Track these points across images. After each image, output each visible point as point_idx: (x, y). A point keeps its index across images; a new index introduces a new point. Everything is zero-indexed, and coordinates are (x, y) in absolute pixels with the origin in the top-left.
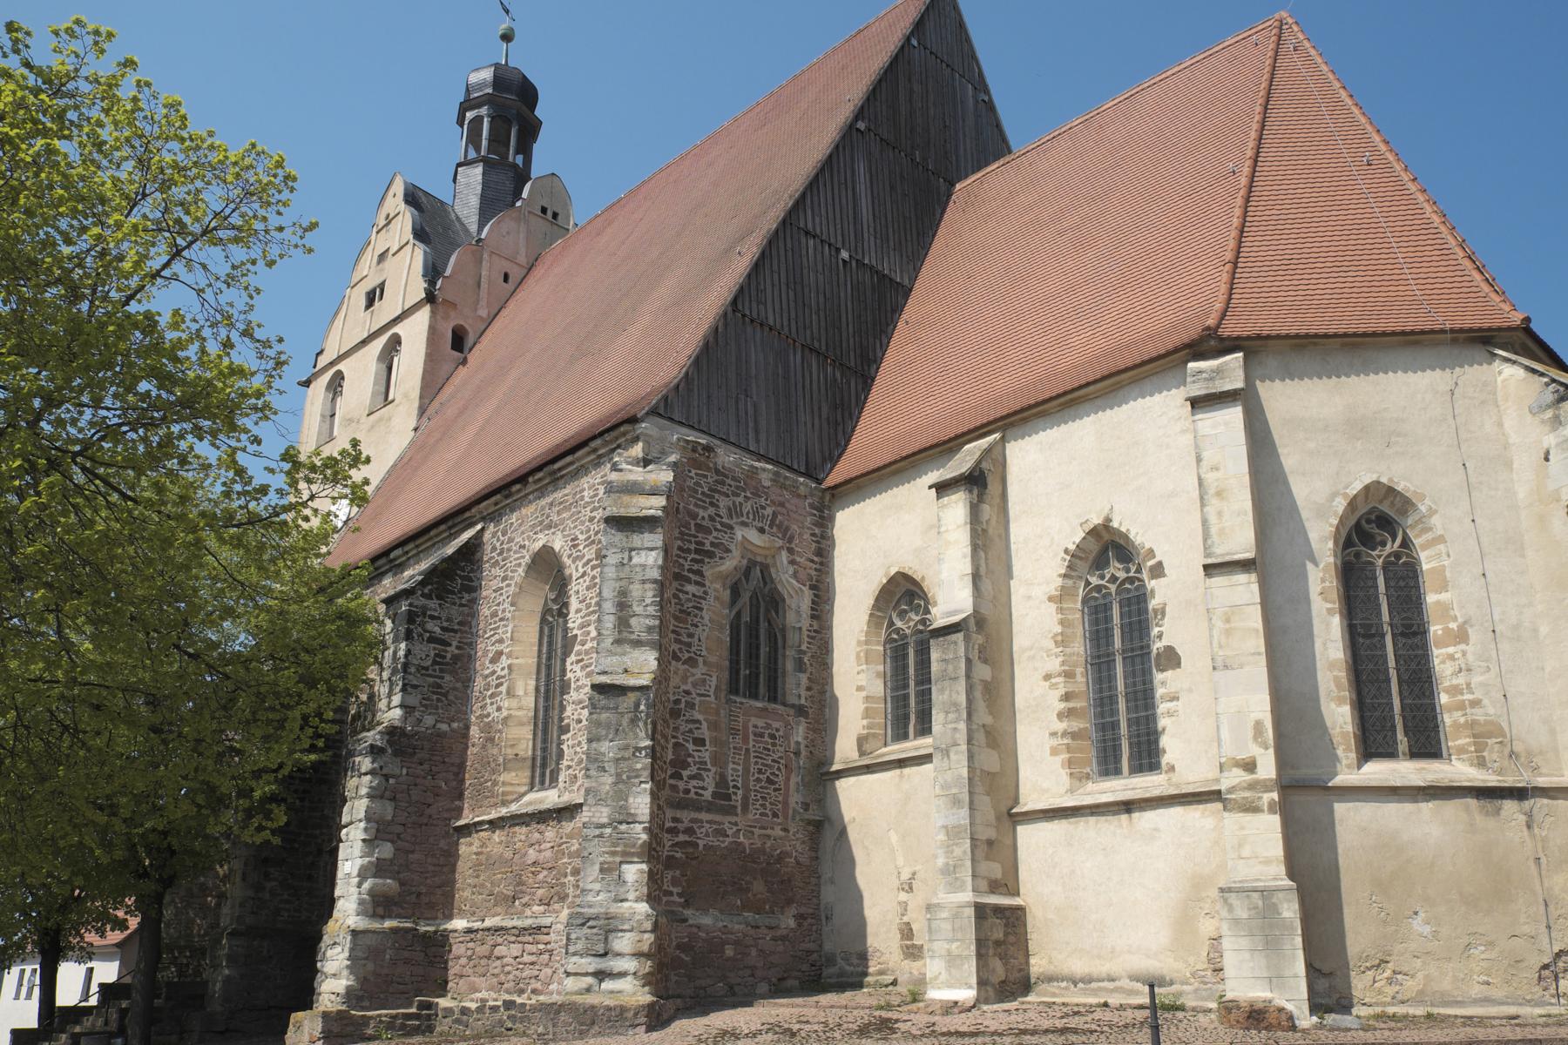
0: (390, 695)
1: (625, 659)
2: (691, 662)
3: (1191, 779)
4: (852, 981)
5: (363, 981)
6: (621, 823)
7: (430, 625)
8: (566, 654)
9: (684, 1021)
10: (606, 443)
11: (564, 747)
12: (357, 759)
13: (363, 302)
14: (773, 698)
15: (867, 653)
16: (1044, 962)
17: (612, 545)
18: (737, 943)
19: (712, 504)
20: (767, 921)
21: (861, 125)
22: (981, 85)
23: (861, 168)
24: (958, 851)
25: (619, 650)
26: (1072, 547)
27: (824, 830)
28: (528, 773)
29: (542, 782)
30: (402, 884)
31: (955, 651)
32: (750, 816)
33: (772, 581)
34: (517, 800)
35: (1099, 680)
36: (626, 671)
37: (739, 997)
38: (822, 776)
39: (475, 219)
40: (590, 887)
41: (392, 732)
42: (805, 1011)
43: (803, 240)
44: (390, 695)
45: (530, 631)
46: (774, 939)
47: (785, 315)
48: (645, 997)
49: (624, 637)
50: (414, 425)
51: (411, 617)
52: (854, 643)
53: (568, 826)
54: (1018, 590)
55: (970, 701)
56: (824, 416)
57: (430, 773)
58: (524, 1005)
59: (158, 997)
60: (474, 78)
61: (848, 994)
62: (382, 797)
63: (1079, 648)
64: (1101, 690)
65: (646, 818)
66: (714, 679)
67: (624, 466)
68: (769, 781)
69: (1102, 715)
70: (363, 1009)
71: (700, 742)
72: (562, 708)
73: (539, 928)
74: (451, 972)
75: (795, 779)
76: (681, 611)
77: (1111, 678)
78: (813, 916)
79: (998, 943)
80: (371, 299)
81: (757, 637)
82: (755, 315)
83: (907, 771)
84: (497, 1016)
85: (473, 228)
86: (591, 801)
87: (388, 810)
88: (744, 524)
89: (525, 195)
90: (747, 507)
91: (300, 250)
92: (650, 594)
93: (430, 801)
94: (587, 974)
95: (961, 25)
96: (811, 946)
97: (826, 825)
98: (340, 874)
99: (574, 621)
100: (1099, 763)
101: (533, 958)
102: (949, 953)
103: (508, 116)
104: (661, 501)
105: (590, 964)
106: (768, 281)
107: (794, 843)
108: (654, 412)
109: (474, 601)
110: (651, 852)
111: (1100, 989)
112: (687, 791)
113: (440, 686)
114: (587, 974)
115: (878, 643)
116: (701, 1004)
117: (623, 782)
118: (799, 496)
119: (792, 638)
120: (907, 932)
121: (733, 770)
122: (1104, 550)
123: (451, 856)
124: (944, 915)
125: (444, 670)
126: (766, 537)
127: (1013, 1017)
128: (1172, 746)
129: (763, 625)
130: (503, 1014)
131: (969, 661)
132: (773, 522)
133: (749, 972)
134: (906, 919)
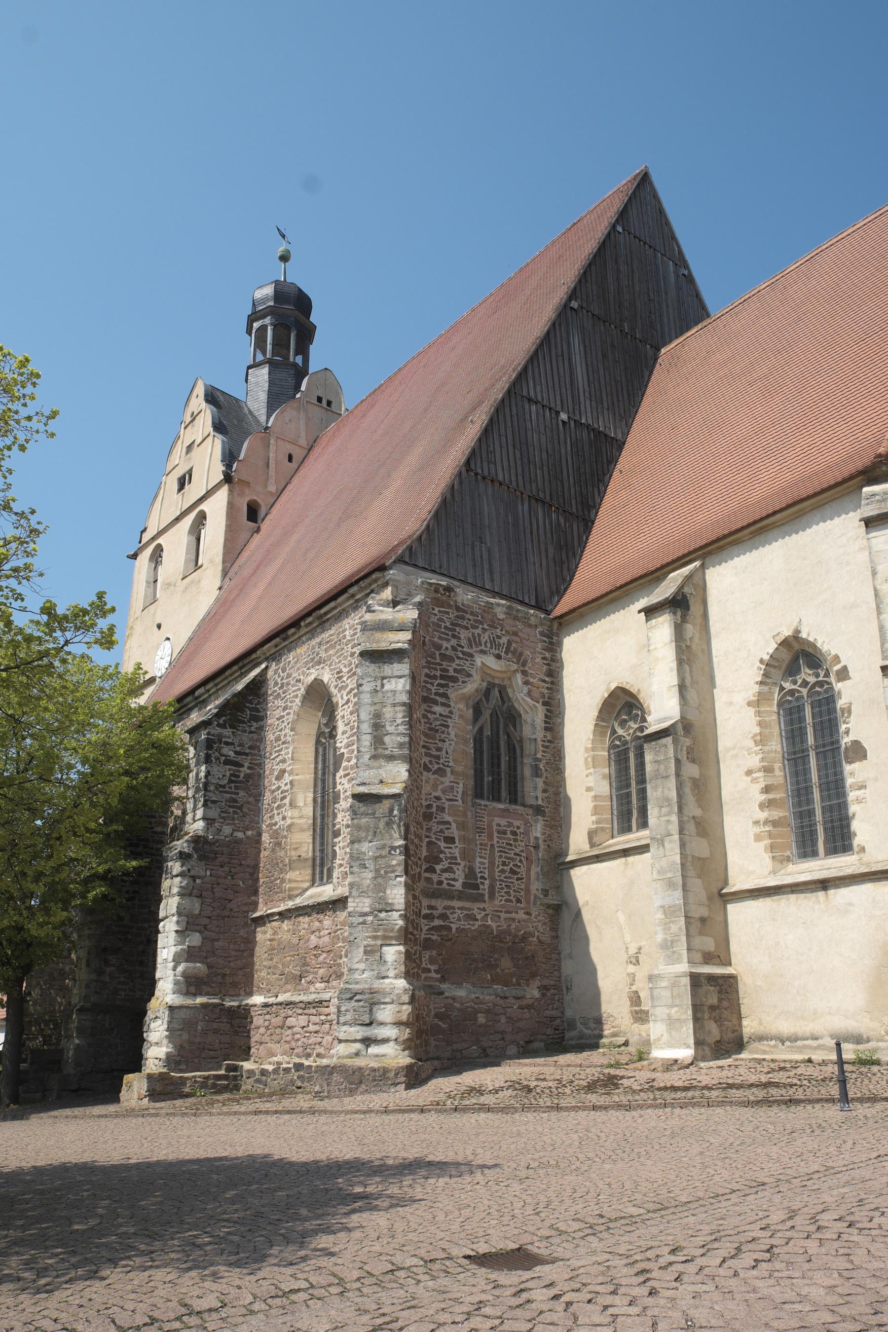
0: (195, 809)
1: (381, 771)
2: (441, 772)
3: (880, 858)
4: (589, 1041)
5: (180, 1048)
6: (380, 911)
7: (226, 750)
8: (336, 770)
9: (440, 1080)
10: (362, 589)
11: (337, 848)
12: (170, 864)
13: (176, 487)
14: (514, 800)
15: (594, 758)
16: (755, 1024)
17: (367, 675)
18: (488, 1012)
19: (454, 636)
20: (514, 992)
21: (574, 304)
22: (681, 262)
23: (576, 341)
24: (674, 928)
25: (376, 764)
26: (766, 657)
27: (562, 911)
28: (309, 871)
29: (322, 879)
30: (210, 967)
31: (666, 753)
32: (497, 902)
33: (509, 699)
34: (301, 894)
35: (795, 774)
36: (382, 782)
37: (489, 1058)
38: (559, 866)
39: (264, 411)
40: (356, 966)
41: (197, 841)
42: (545, 1070)
43: (527, 406)
44: (195, 809)
45: (307, 751)
46: (521, 1008)
47: (513, 471)
48: (405, 1059)
49: (380, 753)
50: (219, 585)
51: (209, 744)
52: (582, 750)
53: (342, 915)
54: (720, 697)
55: (680, 796)
56: (551, 556)
57: (231, 874)
58: (310, 1067)
59: (25, 1061)
60: (259, 294)
61: (585, 1054)
62: (190, 895)
63: (776, 745)
64: (798, 783)
65: (402, 906)
66: (461, 785)
67: (377, 608)
68: (512, 872)
69: (799, 804)
70: (181, 1071)
71: (450, 840)
72: (335, 816)
73: (321, 1002)
74: (253, 1040)
75: (535, 870)
76: (430, 729)
77: (806, 771)
78: (555, 987)
79: (712, 1008)
80: (182, 483)
81: (498, 748)
82: (486, 473)
83: (631, 859)
84: (289, 1077)
85: (263, 419)
86: (355, 893)
87: (196, 906)
88: (483, 652)
89: (303, 388)
90: (485, 637)
91: (44, 435)
92: (400, 715)
93: (231, 897)
94: (355, 1041)
95: (661, 211)
96: (554, 1013)
97: (564, 908)
98: (159, 960)
99: (341, 741)
100: (798, 847)
101: (317, 1028)
102: (669, 1017)
103: (289, 321)
104: (407, 636)
105: (358, 1032)
106: (497, 443)
107: (535, 924)
108: (400, 560)
109: (261, 729)
110: (407, 936)
111: (805, 1047)
112: (440, 883)
113: (235, 801)
114: (355, 1041)
115: (603, 749)
116: (455, 1065)
117: (381, 877)
118: (530, 626)
119: (529, 748)
120: (635, 999)
121: (480, 863)
122: (795, 659)
123: (250, 943)
124: (664, 984)
125: (239, 787)
126: (502, 662)
127: (725, 1073)
128: (862, 829)
129: (503, 738)
130: (294, 1075)
131: (678, 762)
132: (508, 648)
133: (500, 1036)
134: (634, 988)
